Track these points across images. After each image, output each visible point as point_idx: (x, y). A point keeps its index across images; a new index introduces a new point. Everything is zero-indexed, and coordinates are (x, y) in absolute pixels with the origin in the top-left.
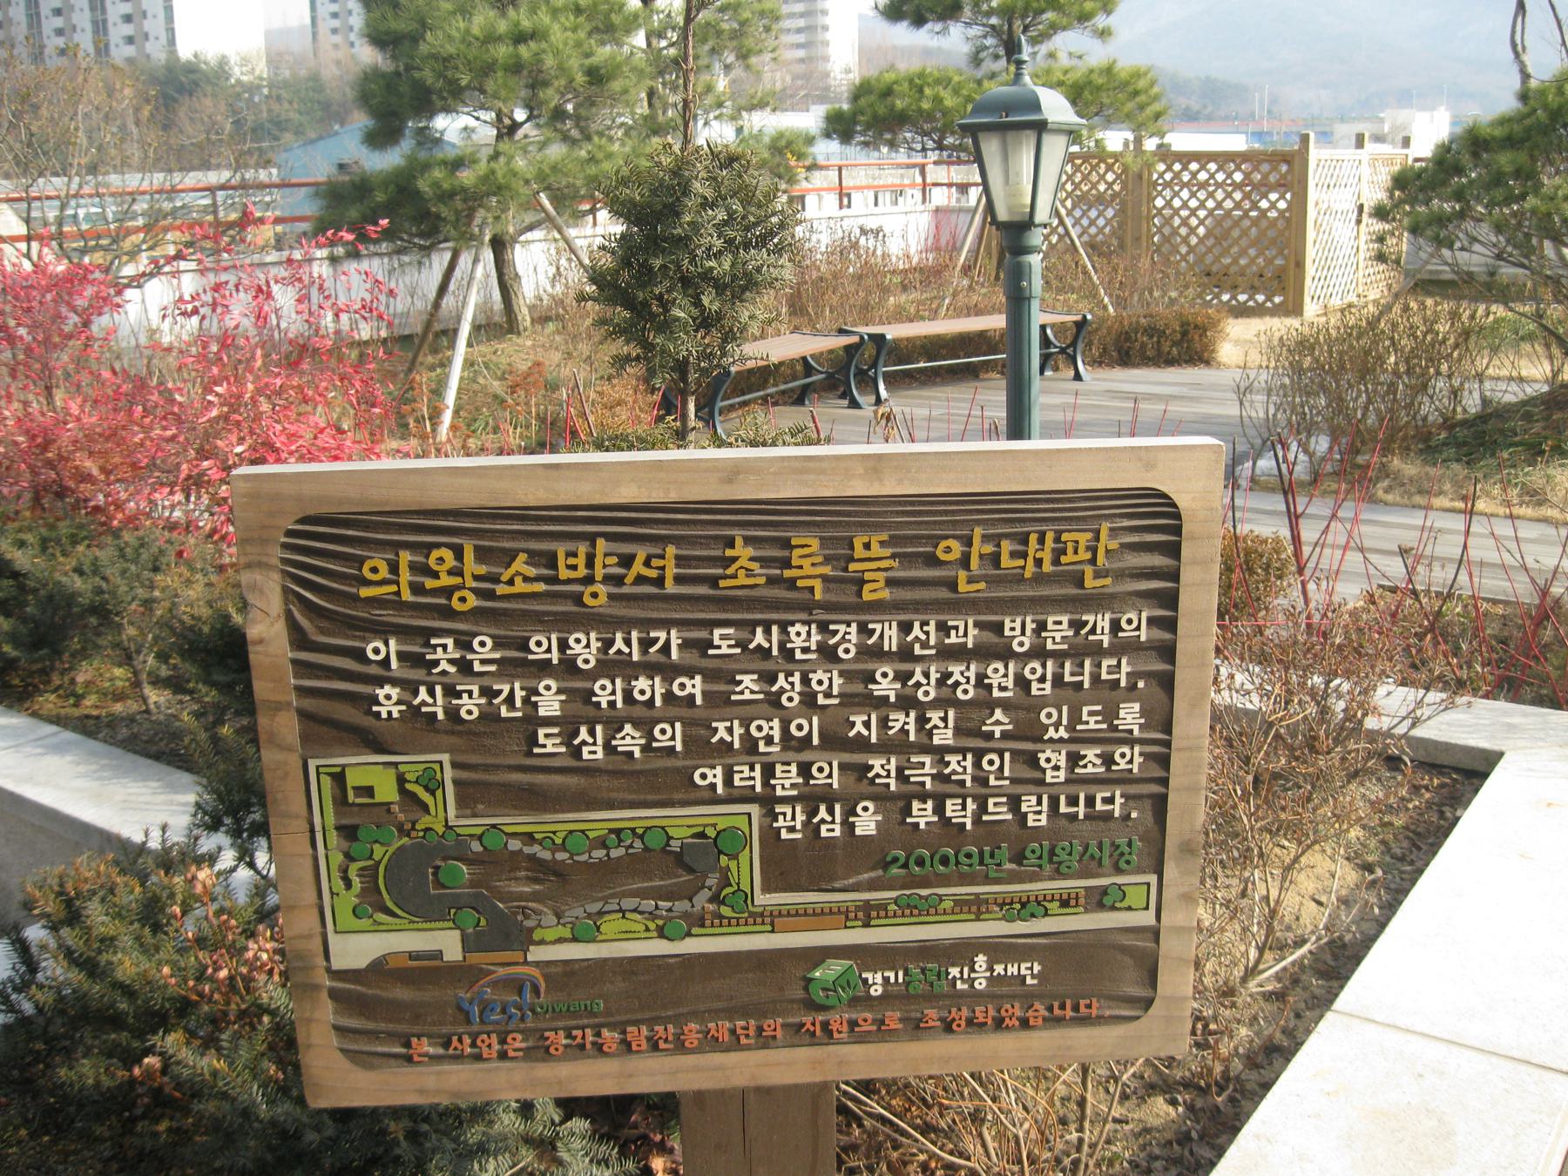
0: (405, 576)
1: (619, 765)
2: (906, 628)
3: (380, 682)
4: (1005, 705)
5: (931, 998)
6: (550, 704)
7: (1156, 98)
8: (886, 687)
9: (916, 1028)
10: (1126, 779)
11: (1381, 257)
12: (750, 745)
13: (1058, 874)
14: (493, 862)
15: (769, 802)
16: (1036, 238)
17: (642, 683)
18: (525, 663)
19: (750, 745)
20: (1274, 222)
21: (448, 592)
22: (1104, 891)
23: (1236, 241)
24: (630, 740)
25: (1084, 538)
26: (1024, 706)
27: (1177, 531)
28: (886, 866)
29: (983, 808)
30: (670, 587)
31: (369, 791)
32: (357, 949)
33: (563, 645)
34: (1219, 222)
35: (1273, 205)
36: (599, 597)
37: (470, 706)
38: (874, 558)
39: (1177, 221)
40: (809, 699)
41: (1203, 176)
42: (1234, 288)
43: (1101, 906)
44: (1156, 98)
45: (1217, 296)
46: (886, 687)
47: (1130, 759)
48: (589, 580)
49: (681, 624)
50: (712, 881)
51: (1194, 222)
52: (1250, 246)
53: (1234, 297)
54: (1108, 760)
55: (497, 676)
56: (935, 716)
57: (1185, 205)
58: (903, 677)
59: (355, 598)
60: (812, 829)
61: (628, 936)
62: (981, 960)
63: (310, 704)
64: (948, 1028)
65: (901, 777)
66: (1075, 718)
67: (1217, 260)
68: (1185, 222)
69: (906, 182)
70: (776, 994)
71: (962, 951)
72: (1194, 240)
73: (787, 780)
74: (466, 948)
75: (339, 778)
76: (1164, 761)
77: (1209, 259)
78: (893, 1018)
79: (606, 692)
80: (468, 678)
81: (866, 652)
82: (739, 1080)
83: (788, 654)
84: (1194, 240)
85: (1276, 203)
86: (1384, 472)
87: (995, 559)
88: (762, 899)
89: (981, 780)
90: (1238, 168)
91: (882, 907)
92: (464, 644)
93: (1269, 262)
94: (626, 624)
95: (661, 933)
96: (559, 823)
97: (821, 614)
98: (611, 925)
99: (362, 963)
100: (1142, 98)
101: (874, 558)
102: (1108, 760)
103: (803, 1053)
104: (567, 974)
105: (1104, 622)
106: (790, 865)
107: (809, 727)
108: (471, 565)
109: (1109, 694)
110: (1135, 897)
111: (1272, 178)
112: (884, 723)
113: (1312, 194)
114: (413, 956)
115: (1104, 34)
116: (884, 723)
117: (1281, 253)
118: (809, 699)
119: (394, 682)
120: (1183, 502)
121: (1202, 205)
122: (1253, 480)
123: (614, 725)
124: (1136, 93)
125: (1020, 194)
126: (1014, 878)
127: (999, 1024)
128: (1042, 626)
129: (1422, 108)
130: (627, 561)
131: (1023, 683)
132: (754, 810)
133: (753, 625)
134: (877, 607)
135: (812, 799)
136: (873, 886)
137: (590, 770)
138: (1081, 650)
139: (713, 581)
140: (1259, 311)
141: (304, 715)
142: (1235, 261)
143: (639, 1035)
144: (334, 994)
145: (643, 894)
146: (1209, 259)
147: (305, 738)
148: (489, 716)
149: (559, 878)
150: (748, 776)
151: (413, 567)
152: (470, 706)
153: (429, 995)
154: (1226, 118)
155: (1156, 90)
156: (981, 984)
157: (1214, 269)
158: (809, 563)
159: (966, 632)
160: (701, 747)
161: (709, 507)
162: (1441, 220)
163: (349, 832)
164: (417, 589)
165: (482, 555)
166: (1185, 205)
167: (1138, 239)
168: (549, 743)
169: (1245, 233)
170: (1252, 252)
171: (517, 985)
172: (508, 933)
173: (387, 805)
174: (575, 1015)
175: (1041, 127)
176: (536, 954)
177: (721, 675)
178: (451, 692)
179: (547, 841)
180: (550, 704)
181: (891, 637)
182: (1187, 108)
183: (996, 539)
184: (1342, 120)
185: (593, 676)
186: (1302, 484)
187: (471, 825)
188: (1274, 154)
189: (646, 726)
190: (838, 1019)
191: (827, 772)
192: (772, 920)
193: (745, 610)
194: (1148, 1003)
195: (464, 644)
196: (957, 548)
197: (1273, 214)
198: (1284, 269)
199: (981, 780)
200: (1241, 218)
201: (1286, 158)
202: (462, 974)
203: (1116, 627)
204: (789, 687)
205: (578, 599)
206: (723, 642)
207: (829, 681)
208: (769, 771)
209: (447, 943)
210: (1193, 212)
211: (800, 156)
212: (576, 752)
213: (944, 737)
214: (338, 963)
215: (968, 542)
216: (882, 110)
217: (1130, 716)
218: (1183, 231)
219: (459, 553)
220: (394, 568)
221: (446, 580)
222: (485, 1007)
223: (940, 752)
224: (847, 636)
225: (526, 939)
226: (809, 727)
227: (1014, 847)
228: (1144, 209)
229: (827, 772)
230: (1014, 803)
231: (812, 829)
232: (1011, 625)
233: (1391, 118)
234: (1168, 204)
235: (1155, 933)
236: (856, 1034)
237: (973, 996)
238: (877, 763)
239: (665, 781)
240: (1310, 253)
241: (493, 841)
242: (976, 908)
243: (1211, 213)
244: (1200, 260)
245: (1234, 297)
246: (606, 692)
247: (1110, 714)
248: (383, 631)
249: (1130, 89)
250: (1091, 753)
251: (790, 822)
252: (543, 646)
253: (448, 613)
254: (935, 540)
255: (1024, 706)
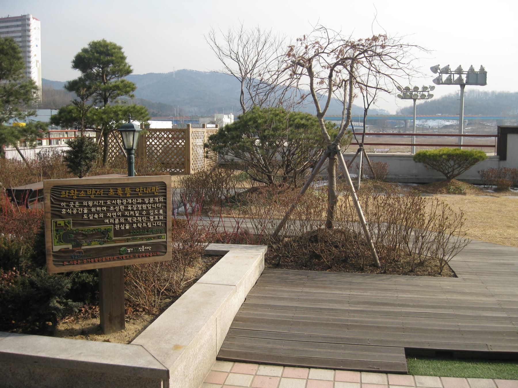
0: (67, 194)
1: (95, 219)
2: (132, 200)
3: (63, 209)
4: (145, 210)
5: (137, 252)
6: (86, 211)
7: (147, 115)
8: (130, 208)
9: (135, 257)
10: (161, 220)
11: (207, 157)
12: (112, 216)
13: (153, 234)
14: (77, 234)
15: (114, 224)
16: (133, 152)
17: (98, 208)
18: (83, 206)
19: (112, 216)
20: (181, 149)
21: (73, 196)
22: (159, 236)
23: (171, 154)
24: (96, 216)
25: (154, 188)
26: (147, 210)
27: (166, 187)
28: (130, 233)
29: (143, 225)
30: (102, 195)
31: (60, 224)
32: (57, 248)
33: (88, 203)
34: (165, 148)
35: (180, 144)
36: (93, 196)
37: (75, 212)
38: (128, 190)
39: (153, 149)
40: (120, 210)
41: (160, 136)
42: (170, 168)
43: (159, 238)
44: (147, 115)
45: (166, 170)
46: (130, 208)
47: (161, 217)
48: (91, 194)
49: (103, 200)
50: (107, 236)
51: (158, 149)
52: (174, 155)
53: (170, 170)
54: (159, 218)
55: (79, 207)
56: (136, 212)
57: (156, 144)
58: (132, 207)
59: (60, 197)
60: (120, 228)
61: (95, 244)
62: (143, 247)
63: (53, 212)
64: (139, 257)
65: (132, 220)
66: (154, 212)
67: (165, 159)
68: (156, 149)
69: (61, 136)
70: (115, 253)
71: (140, 245)
72: (159, 154)
73: (117, 221)
74: (73, 247)
75: (56, 223)
76: (166, 218)
77: (163, 159)
78: (131, 256)
79: (93, 209)
80: (75, 208)
81: (127, 203)
82: (110, 266)
83: (117, 204)
84: (159, 154)
85: (181, 142)
86: (210, 209)
87: (143, 191)
88: (114, 238)
89: (142, 221)
90: (170, 133)
91: (130, 239)
92: (75, 203)
93: (180, 160)
94: (96, 200)
95: (100, 244)
96: (87, 228)
97: (121, 198)
98: (93, 243)
99: (58, 250)
100: (143, 115)
101: (128, 190)
102: (159, 218)
103: (119, 261)
104: (87, 251)
105: (157, 199)
106: (118, 233)
107: (120, 214)
108: (76, 192)
109: (158, 209)
110: (163, 237)
111: (180, 136)
112: (129, 213)
113: (191, 141)
114: (65, 249)
115: (132, 96)
116: (129, 213)
117: (183, 157)
118: (120, 210)
119: (65, 209)
120: (166, 183)
121: (160, 144)
122: (178, 213)
123: (94, 214)
124: (142, 113)
125: (130, 143)
126: (147, 234)
127: (146, 256)
128: (149, 200)
129: (226, 114)
130: (96, 192)
131: (147, 207)
132: (112, 225)
133: (112, 200)
134: (129, 197)
135: (120, 224)
136: (128, 236)
137: (91, 220)
138: (155, 203)
139: (107, 194)
140: (178, 174)
141: (52, 214)
142: (171, 159)
143: (96, 260)
144: (53, 255)
145: (97, 238)
146: (163, 159)
147: (52, 217)
148: (77, 213)
149: (85, 236)
150: (112, 221)
151: (68, 193)
152: (75, 212)
153: (67, 254)
154: (165, 116)
155: (147, 112)
156: (143, 250)
157: (165, 162)
158: (120, 192)
159: (140, 200)
160: (106, 217)
161: (107, 184)
162: (221, 148)
163: (57, 230)
164: (68, 196)
165: (77, 191)
166: (156, 144)
167: (142, 154)
168: (85, 217)
169: (173, 151)
170: (175, 157)
171: (79, 252)
172: (78, 245)
173: (62, 226)
174: (87, 256)
175: (134, 131)
176: (83, 248)
177: (108, 207)
178: (72, 210)
179: (85, 231)
180: (86, 211)
181: (130, 202)
182: (153, 113)
183: (143, 188)
184: (202, 117)
185: (91, 207)
186: (190, 213)
187: (75, 229)
188: (180, 130)
189: (98, 214)
190: (124, 256)
191: (122, 220)
192: (115, 241)
193: (112, 198)
194: (166, 253)
195: (75, 203)
196: (138, 190)
197: (180, 146)
198: (184, 161)
199: (142, 221)
200: (172, 147)
201: (183, 131)
202: (72, 251)
203: (159, 199)
204: (117, 208)
205: (90, 197)
206: (109, 202)
207: (122, 207)
208: (114, 220)
209: (70, 246)
210: (158, 146)
211: (44, 130)
212: (89, 218)
213: (137, 215)
214: (54, 250)
215: (140, 188)
216: (68, 117)
217: (161, 211)
218: (155, 151)
219: (74, 191)
220: (66, 193)
221: (72, 194)
222: (75, 256)
223: (137, 217)
224: (125, 201)
225: (81, 245)
226: (120, 214)
227: (147, 230)
228: (144, 145)
229: (122, 220)
230: (147, 224)
231: (120, 228)
232: (146, 200)
233: (217, 116)
234: (151, 143)
235: (166, 242)
236: (127, 259)
237: (142, 252)
238: (129, 218)
239: (101, 221)
240: (191, 157)
241: (77, 231)
242: (142, 239)
243: (163, 146)
244: (161, 159)
245: (170, 170)
246: (93, 209)
247: (159, 211)
248: (63, 201)
249: (140, 112)
250: (156, 217)
251: (117, 227)
252: (85, 203)
253: (73, 199)
254: (136, 188)
255: (147, 210)
